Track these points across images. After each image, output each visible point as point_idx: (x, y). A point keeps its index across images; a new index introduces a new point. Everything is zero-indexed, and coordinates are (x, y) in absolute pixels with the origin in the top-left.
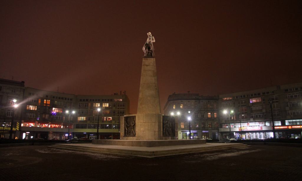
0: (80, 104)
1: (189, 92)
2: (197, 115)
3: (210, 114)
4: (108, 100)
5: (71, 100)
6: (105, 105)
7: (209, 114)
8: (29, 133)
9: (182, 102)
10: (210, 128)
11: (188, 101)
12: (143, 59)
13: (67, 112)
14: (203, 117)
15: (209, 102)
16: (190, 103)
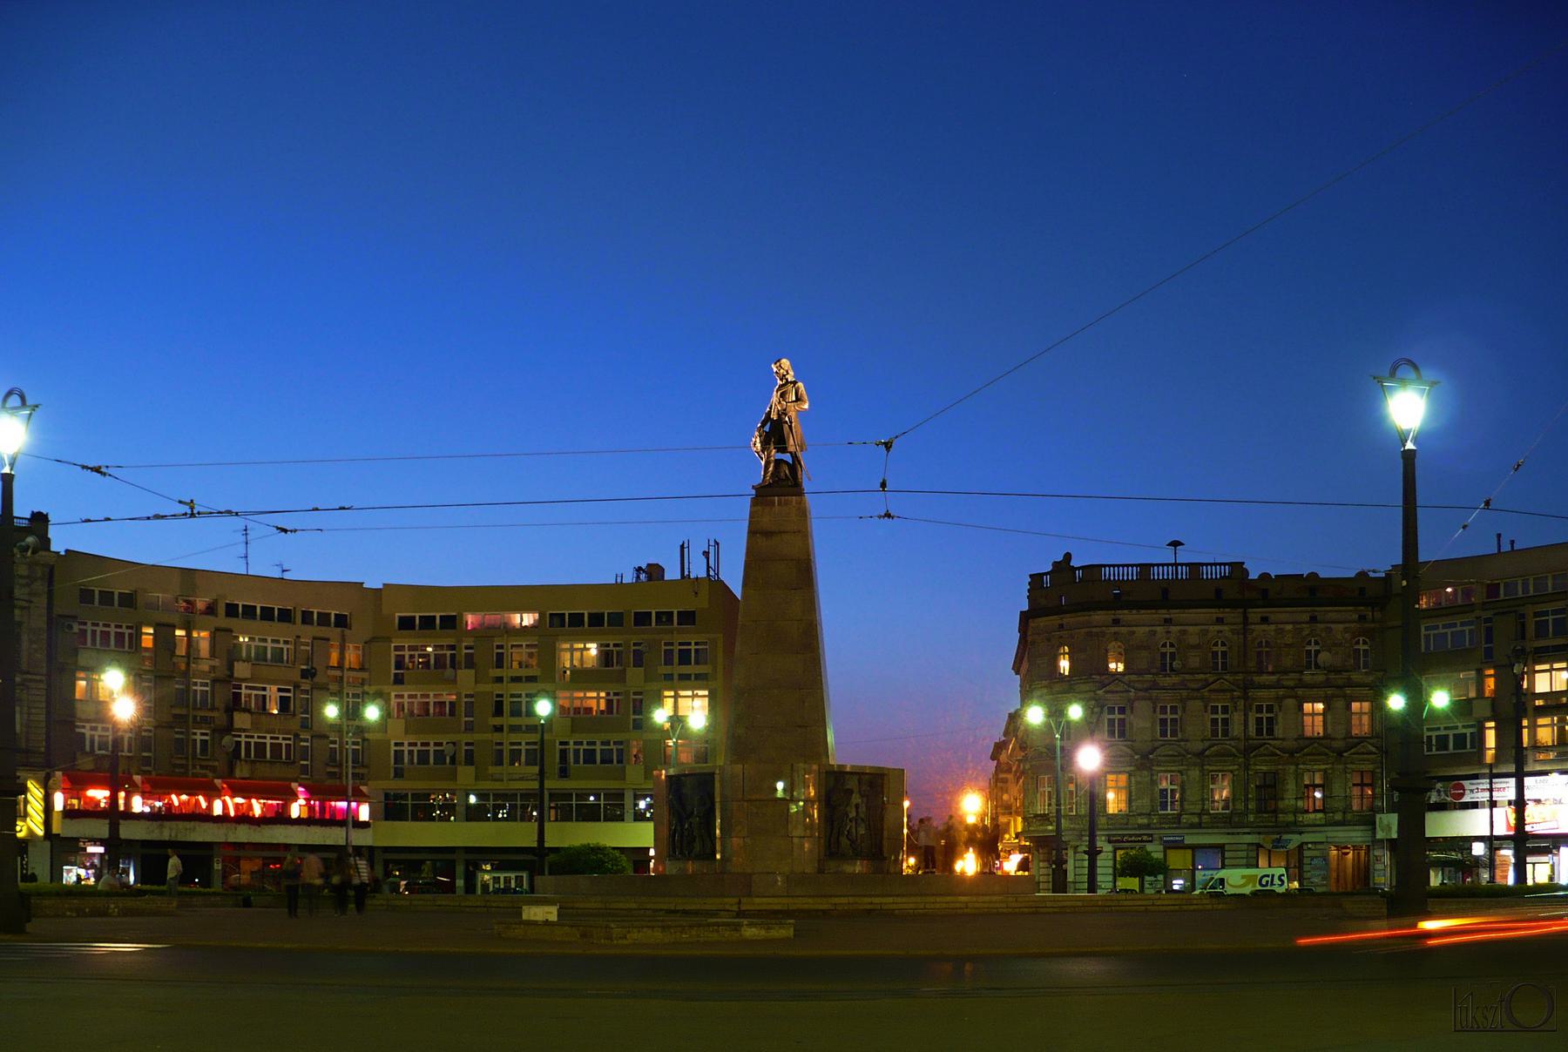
0: (407, 653)
1: (1175, 544)
2: (1122, 722)
3: (1320, 706)
4: (596, 620)
5: (342, 621)
6: (577, 655)
7: (1313, 714)
8: (101, 850)
9: (1116, 622)
10: (1315, 811)
11: (1163, 614)
12: (733, 577)
13: (1396, 702)
14: (1270, 731)
15: (1313, 619)
16: (1173, 629)
